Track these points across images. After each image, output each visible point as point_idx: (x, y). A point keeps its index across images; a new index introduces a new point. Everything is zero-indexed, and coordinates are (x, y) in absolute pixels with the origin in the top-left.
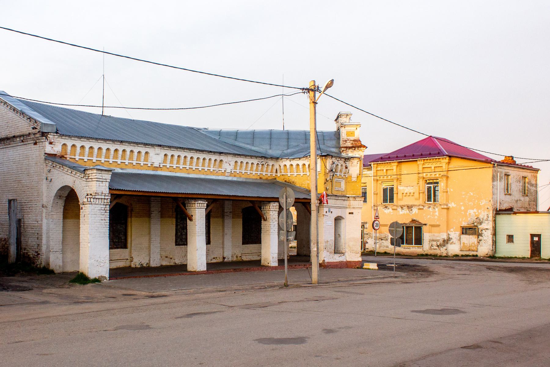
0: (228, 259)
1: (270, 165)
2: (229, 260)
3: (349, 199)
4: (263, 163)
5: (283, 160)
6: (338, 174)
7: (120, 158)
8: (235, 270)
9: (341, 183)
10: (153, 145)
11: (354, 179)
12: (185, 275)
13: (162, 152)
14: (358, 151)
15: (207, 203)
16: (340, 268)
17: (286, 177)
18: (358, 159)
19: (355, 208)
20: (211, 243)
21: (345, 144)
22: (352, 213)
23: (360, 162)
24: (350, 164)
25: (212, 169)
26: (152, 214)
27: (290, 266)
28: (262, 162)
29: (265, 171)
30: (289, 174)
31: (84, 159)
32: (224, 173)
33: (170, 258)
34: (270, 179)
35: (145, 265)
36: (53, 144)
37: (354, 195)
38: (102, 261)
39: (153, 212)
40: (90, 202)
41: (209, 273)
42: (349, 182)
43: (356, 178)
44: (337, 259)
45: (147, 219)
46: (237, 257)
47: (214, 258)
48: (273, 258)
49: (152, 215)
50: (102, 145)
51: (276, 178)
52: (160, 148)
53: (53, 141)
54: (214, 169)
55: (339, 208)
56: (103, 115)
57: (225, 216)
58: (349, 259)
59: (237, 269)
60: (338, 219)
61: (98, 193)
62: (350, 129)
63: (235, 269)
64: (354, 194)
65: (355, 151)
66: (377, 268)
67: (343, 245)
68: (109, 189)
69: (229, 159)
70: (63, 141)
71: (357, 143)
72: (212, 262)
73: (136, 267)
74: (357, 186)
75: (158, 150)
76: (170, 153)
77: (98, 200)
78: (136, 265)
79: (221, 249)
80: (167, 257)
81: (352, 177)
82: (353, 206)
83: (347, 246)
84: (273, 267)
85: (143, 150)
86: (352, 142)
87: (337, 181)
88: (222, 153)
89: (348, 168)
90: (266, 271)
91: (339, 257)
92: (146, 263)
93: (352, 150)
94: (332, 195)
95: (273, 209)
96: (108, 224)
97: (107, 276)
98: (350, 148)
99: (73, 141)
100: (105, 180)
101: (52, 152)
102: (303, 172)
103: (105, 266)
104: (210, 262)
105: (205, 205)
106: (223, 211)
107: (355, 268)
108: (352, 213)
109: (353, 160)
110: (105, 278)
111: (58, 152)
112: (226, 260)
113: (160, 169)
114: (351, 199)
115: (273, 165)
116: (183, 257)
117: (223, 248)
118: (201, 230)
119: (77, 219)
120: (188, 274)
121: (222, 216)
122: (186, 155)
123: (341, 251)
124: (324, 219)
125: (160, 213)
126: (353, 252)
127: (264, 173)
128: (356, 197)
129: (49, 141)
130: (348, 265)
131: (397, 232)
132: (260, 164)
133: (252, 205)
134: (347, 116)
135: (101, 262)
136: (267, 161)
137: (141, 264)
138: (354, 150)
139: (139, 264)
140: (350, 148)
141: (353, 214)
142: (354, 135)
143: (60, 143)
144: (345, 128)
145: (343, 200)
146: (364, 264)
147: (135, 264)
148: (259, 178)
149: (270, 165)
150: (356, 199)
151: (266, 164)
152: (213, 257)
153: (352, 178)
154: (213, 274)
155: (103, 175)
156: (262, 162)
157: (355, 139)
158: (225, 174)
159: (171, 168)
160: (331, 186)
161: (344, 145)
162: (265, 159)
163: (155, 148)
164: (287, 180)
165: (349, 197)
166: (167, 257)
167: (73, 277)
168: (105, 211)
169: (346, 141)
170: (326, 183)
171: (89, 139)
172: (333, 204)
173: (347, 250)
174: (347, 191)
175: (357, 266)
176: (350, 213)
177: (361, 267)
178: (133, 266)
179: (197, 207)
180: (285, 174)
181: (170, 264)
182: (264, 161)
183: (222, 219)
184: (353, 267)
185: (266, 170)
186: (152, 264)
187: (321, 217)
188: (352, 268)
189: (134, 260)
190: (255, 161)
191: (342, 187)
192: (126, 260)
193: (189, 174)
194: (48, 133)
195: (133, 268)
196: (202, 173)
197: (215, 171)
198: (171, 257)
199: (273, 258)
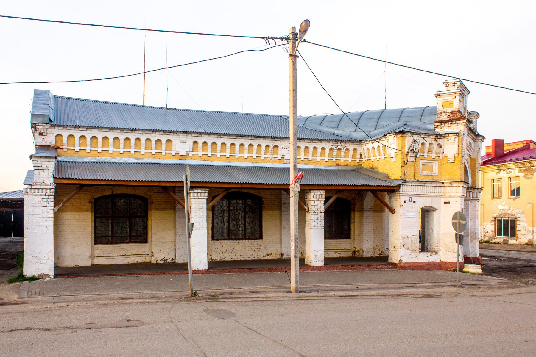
1: (350, 149)
3: (443, 185)
4: (339, 147)
5: (366, 143)
6: (426, 155)
7: (165, 149)
8: (271, 270)
10: (175, 132)
11: (451, 161)
13: (191, 139)
14: (457, 124)
15: (208, 192)
16: (428, 270)
17: (370, 162)
18: (455, 135)
19: (451, 196)
20: (264, 238)
21: (440, 117)
22: (448, 203)
23: (459, 138)
24: (445, 142)
25: (263, 156)
26: (177, 206)
27: (343, 266)
28: (338, 146)
29: (343, 156)
30: (372, 158)
31: (86, 150)
32: (281, 161)
34: (352, 165)
35: (169, 261)
36: (43, 135)
37: (451, 180)
38: (43, 257)
40: (27, 192)
41: (210, 273)
42: (444, 164)
43: (454, 159)
44: (424, 258)
45: (172, 211)
47: (268, 255)
48: (316, 256)
50: (244, 141)
51: (361, 165)
53: (43, 132)
54: (266, 156)
55: (428, 197)
56: (168, 107)
57: (283, 208)
58: (444, 259)
59: (255, 268)
60: (426, 212)
61: (36, 183)
62: (447, 98)
63: (251, 269)
64: (451, 179)
65: (452, 125)
66: (480, 271)
67: (436, 241)
68: (54, 177)
69: (286, 144)
70: (57, 132)
71: (455, 115)
72: (265, 258)
73: (157, 263)
74: (455, 168)
75: (183, 137)
76: (200, 140)
77: (36, 190)
78: (157, 261)
79: (279, 245)
82: (449, 194)
83: (441, 243)
84: (314, 267)
85: (164, 138)
86: (448, 114)
87: (423, 163)
88: (276, 138)
89: (442, 147)
90: (303, 271)
91: (428, 256)
92: (171, 259)
93: (449, 124)
94: (415, 180)
95: (316, 198)
96: (53, 216)
97: (52, 273)
98: (445, 122)
99: (69, 131)
100: (46, 168)
101: (44, 143)
102: (385, 155)
103: (47, 263)
104: (262, 259)
105: (206, 194)
106: (280, 203)
107: (450, 270)
108: (448, 203)
109: (449, 136)
110: (48, 276)
111: (51, 143)
112: (284, 257)
113: (190, 157)
114: (446, 185)
115: (355, 150)
116: (224, 253)
117: (281, 243)
118: (199, 223)
119: (78, 212)
120: (177, 273)
122: (72, 133)
123: (433, 250)
124: (401, 210)
126: (449, 250)
127: (342, 159)
128: (452, 183)
129: (38, 132)
130: (441, 266)
131: (460, 225)
132: (335, 148)
133: (226, 192)
134: (455, 84)
135: (42, 258)
136: (345, 145)
138: (450, 124)
139: (162, 259)
140: (445, 122)
142: (453, 105)
143: (54, 134)
144: (440, 97)
145: (435, 186)
146: (465, 267)
147: (156, 260)
148: (335, 165)
149: (350, 150)
150: (453, 185)
151: (344, 148)
152: (265, 253)
153: (448, 159)
154: (216, 273)
155: (43, 163)
156: (338, 146)
157: (453, 110)
158: (283, 161)
159: (204, 157)
160: (413, 169)
161: (439, 118)
162: (342, 143)
163: (179, 135)
164: (371, 166)
165: (443, 183)
167: (427, 267)
168: (47, 203)
169: (441, 113)
170: (403, 166)
171: (90, 129)
172: (434, 192)
173: (442, 248)
174: (442, 175)
175: (454, 268)
176: (445, 203)
177: (461, 270)
178: (153, 261)
179: (194, 197)
180: (369, 159)
182: (341, 145)
183: (279, 212)
184: (448, 269)
185: (345, 156)
186: (178, 260)
187: (398, 208)
188: (447, 270)
189: (155, 256)
190: (328, 146)
191: (434, 171)
192: (146, 255)
193: (230, 162)
194: (36, 123)
195: (153, 264)
196: (250, 161)
197: (268, 158)
199: (316, 256)
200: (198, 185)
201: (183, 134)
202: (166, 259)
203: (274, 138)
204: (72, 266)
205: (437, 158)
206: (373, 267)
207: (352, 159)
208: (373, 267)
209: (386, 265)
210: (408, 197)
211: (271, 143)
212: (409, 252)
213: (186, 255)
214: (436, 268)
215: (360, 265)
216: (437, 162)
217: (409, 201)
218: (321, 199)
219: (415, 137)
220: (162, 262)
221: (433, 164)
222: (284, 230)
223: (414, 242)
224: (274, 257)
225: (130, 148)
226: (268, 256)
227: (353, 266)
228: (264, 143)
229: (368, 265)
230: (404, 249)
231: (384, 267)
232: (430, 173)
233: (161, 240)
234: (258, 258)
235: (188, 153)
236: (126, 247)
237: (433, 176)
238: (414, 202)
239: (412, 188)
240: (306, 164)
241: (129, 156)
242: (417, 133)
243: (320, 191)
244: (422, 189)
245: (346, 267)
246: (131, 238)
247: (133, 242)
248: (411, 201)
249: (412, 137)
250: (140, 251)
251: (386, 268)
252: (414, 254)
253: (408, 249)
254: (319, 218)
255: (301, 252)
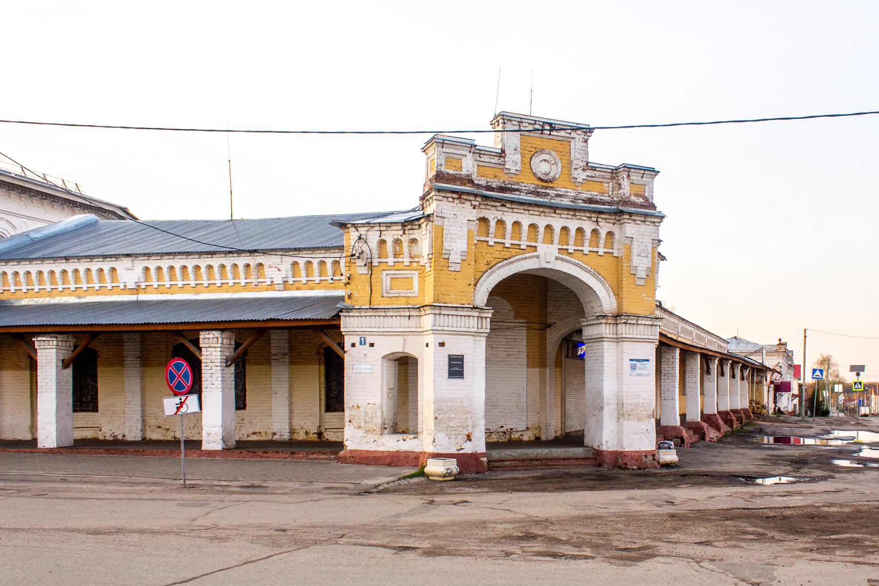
0: (282, 436)
2: (283, 437)
9: (412, 278)
12: (9, 452)
13: (140, 264)
20: (247, 407)
25: (243, 281)
27: (248, 451)
33: (166, 429)
35: (120, 437)
39: (128, 357)
46: (307, 433)
47: (254, 433)
49: (125, 362)
52: (130, 259)
55: (397, 335)
72: (250, 439)
75: (126, 262)
76: (152, 264)
78: (105, 437)
80: (159, 427)
81: (450, 260)
85: (106, 266)
104: (246, 439)
113: (143, 290)
121: (266, 359)
125: (139, 359)
137: (114, 436)
141: (439, 343)
152: (250, 432)
153: (450, 265)
154: (62, 453)
159: (297, 285)
160: (368, 288)
166: (159, 427)
167: (388, 460)
172: (467, 326)
178: (101, 438)
181: (166, 439)
193: (197, 293)
198: (167, 427)
200: (44, 330)
201: (128, 259)
202: (115, 434)
203: (253, 252)
204: (11, 439)
205: (415, 264)
206: (301, 456)
207: (307, 279)
208: (301, 456)
209: (324, 454)
210: (359, 337)
211: (253, 261)
212: (361, 432)
213: (137, 429)
214: (408, 463)
215: (277, 452)
216: (417, 273)
217: (361, 344)
218: (216, 345)
219: (362, 230)
220: (111, 438)
221: (411, 276)
222: (276, 395)
223: (370, 415)
224: (264, 438)
225: (188, 279)
226: (255, 436)
227: (265, 452)
228: (241, 261)
229: (293, 453)
230: (352, 427)
231: (321, 456)
232: (404, 293)
233: (111, 409)
234: (240, 438)
235: (285, 280)
236: (80, 417)
237: (408, 297)
238: (372, 345)
239: (451, 321)
240: (312, 289)
241: (70, 295)
242: (363, 225)
243: (214, 332)
244: (461, 320)
245: (253, 455)
246: (81, 405)
247: (83, 411)
248: (365, 344)
249: (358, 231)
250: (89, 422)
251: (325, 459)
252: (370, 437)
253: (359, 427)
254: (213, 375)
255: (306, 431)
